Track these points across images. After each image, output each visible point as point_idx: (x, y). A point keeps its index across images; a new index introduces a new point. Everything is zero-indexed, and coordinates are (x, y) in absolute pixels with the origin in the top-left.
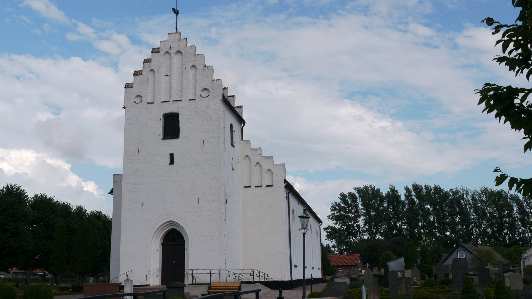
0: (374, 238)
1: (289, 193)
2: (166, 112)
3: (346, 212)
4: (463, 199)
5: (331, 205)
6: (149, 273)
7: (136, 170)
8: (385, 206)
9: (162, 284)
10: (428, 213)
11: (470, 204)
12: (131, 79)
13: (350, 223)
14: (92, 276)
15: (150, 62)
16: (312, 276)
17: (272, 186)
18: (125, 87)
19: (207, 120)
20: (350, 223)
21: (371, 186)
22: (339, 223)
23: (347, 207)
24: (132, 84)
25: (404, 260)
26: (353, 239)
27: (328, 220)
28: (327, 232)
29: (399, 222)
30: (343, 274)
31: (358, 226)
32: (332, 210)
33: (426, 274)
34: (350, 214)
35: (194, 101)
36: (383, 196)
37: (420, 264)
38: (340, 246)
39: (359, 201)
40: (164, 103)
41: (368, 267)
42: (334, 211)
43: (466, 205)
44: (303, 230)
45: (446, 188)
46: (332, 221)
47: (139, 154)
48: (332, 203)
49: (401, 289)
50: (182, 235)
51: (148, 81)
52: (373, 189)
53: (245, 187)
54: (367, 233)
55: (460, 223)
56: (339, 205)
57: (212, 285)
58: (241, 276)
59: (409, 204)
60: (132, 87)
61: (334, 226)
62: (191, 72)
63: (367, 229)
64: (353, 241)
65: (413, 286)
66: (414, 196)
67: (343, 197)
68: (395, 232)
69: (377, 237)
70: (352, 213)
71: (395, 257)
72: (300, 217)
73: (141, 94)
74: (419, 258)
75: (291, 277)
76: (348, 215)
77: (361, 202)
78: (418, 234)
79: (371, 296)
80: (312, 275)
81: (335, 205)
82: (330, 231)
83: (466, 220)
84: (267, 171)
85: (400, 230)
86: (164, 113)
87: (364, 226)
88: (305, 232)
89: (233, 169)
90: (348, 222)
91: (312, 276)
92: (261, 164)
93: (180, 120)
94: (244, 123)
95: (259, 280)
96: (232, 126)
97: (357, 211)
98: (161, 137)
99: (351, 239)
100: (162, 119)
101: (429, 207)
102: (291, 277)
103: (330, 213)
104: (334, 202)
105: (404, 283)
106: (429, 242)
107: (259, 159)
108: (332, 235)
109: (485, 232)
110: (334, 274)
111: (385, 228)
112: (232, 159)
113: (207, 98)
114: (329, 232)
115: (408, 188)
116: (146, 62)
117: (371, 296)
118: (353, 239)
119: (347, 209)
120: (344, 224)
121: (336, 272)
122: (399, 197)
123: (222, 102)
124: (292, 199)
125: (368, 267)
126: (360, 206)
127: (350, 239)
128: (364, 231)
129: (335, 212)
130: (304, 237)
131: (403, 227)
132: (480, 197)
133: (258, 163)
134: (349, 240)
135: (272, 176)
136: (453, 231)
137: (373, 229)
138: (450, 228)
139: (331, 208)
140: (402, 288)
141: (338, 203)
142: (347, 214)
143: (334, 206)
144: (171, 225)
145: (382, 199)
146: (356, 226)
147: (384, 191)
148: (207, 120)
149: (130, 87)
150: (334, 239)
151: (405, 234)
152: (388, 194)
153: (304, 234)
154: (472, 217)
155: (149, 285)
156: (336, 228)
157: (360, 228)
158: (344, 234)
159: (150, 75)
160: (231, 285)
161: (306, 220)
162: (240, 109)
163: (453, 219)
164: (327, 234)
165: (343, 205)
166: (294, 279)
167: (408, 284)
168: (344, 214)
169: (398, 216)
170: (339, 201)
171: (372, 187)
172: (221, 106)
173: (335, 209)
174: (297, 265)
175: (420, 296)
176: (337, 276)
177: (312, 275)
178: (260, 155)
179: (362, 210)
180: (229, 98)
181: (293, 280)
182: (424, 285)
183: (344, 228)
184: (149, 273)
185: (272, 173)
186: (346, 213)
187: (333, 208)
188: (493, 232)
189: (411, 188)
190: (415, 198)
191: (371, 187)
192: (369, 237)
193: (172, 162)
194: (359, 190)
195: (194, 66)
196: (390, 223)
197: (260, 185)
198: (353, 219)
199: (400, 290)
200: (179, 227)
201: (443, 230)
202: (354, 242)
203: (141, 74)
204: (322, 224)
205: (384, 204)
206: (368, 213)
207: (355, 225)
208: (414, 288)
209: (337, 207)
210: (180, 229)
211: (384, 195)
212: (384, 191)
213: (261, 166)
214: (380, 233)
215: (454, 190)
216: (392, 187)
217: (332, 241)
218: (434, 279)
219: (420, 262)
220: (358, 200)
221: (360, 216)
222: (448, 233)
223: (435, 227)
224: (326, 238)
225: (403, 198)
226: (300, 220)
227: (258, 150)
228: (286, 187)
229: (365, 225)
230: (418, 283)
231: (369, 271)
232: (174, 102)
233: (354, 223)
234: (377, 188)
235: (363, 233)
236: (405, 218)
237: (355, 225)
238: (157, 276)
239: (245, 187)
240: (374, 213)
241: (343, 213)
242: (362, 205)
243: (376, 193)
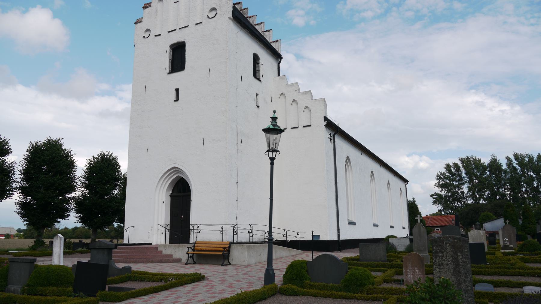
0: (478, 203)
1: (334, 135)
2: (172, 43)
3: (450, 180)
5: (436, 175)
6: (151, 230)
7: (143, 112)
8: (488, 174)
9: (169, 243)
10: (531, 179)
13: (455, 190)
16: (313, 234)
17: (310, 126)
19: (214, 44)
20: (455, 190)
22: (444, 190)
23: (452, 176)
25: (503, 220)
26: (458, 203)
27: (434, 187)
28: (434, 198)
29: (502, 188)
30: (439, 234)
31: (462, 193)
32: (437, 179)
33: (528, 234)
34: (454, 182)
35: (201, 24)
36: (485, 165)
37: (522, 224)
38: (446, 210)
39: (462, 170)
40: (171, 33)
41: (419, 221)
42: (439, 180)
44: (270, 153)
46: (438, 188)
47: (145, 94)
48: (438, 173)
49: (442, 264)
50: (186, 181)
51: (157, 12)
52: (475, 160)
54: (471, 199)
56: (444, 174)
57: (196, 245)
58: (192, 230)
60: (141, 22)
61: (439, 193)
63: (471, 195)
64: (458, 206)
65: (502, 251)
66: (516, 164)
67: (448, 167)
68: (498, 197)
69: (481, 202)
70: (456, 181)
71: (495, 218)
72: (265, 130)
73: (150, 28)
74: (521, 219)
75: (339, 236)
76: (452, 183)
77: (464, 171)
78: (521, 199)
79: (409, 270)
80: (313, 232)
81: (440, 174)
82: (436, 197)
84: (280, 95)
85: (504, 195)
86: (171, 44)
87: (468, 193)
88: (274, 156)
89: (258, 107)
90: (453, 190)
91: (313, 234)
92: (297, 102)
93: (186, 49)
94: (281, 58)
95: (336, 238)
96: (256, 59)
97: (461, 179)
98: (168, 71)
99: (456, 204)
100: (168, 51)
101: (532, 173)
102: (339, 236)
103: (436, 182)
105: (448, 250)
106: (533, 206)
107: (295, 96)
108: (438, 201)
110: (430, 234)
111: (488, 194)
112: (257, 95)
113: (214, 18)
114: (435, 198)
115: (509, 158)
117: (409, 270)
118: (458, 203)
119: (452, 177)
120: (449, 191)
121: (431, 232)
122: (500, 166)
123: (233, 22)
124: (339, 141)
125: (419, 221)
126: (464, 175)
127: (455, 203)
128: (467, 197)
129: (441, 180)
130: (272, 164)
131: (507, 192)
133: (294, 100)
134: (454, 205)
135: (311, 114)
137: (476, 195)
139: (437, 177)
140: (444, 262)
141: (442, 173)
142: (452, 182)
143: (440, 175)
144: (176, 172)
145: (484, 168)
146: (460, 193)
147: (486, 161)
148: (214, 44)
149: (139, 22)
150: (440, 204)
151: (508, 199)
153: (272, 159)
155: (151, 244)
156: (442, 194)
157: (464, 194)
158: (449, 200)
160: (208, 245)
161: (273, 137)
162: (277, 44)
164: (433, 200)
165: (447, 174)
166: (342, 238)
167: (459, 254)
168: (449, 182)
169: (501, 182)
170: (444, 171)
171: (474, 158)
172: (233, 29)
173: (440, 178)
174: (405, 227)
175: (510, 270)
176: (432, 236)
177: (313, 232)
178: (296, 90)
179: (466, 178)
180: (265, 32)
181: (341, 239)
182: (521, 250)
183: (449, 194)
184: (151, 230)
185: (310, 110)
186: (450, 182)
187: (438, 177)
189: (512, 158)
190: (517, 166)
191: (473, 158)
192: (472, 202)
193: (177, 99)
194: (463, 161)
196: (493, 190)
197: (297, 126)
198: (458, 186)
199: (439, 268)
200: (183, 173)
202: (459, 207)
204: (407, 183)
205: (487, 172)
206: (471, 181)
207: (459, 192)
208: (504, 254)
209: (442, 176)
210: (185, 177)
211: (486, 164)
212: (486, 161)
213: (297, 104)
214: (483, 198)
216: (494, 157)
217: (438, 206)
218: (538, 241)
219: (523, 222)
220: (462, 170)
221: (463, 184)
224: (433, 203)
225: (504, 167)
226: (266, 135)
227: (293, 85)
228: (327, 126)
229: (469, 191)
230: (512, 246)
231: (422, 228)
232: (180, 30)
233: (458, 190)
234: (478, 159)
235: (467, 199)
236: (508, 185)
237: (459, 192)
238: (162, 233)
240: (477, 181)
241: (448, 181)
242: (465, 174)
243: (477, 163)
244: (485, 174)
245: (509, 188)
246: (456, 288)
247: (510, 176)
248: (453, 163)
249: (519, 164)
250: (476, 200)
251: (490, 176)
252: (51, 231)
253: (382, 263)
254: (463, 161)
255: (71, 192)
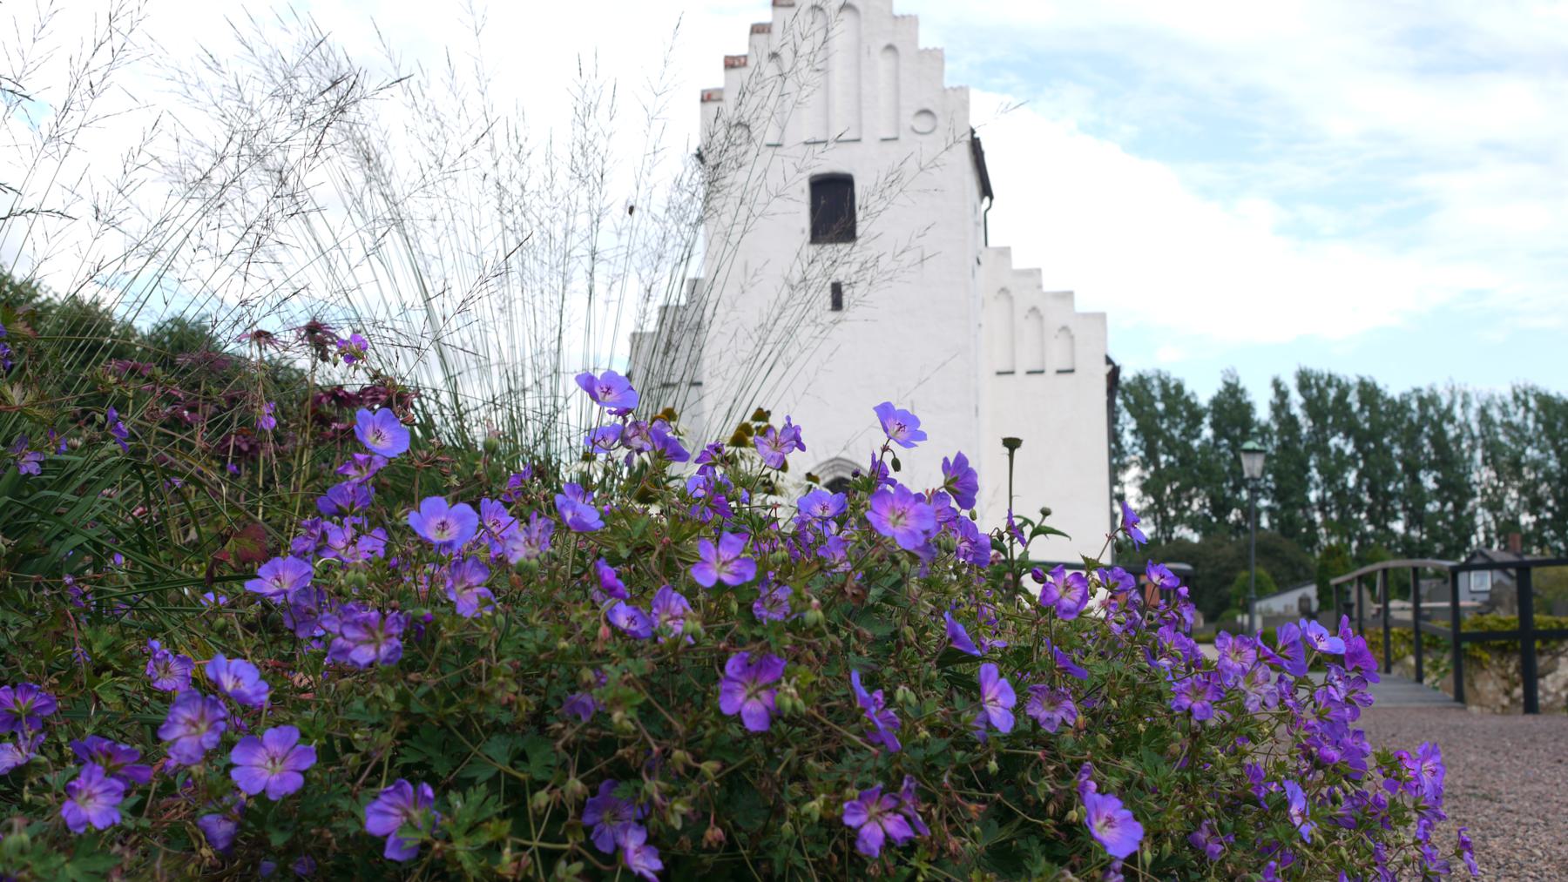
4: (1452, 420)
10: (1343, 462)
11: (1473, 438)
12: (716, 78)
14: (1424, 508)
15: (769, 31)
17: (1072, 371)
18: (703, 100)
21: (1159, 372)
24: (720, 91)
43: (1458, 439)
45: (1394, 387)
52: (1164, 384)
53: (999, 373)
55: (1437, 494)
59: (1280, 433)
62: (883, 64)
71: (1274, 588)
83: (1456, 488)
104: (788, 418)
109: (1516, 523)
116: (758, 32)
122: (1248, 408)
132: (1505, 413)
136: (1416, 518)
138: (1405, 509)
145: (1195, 416)
147: (1204, 391)
152: (1217, 403)
154: (1475, 477)
159: (770, 70)
163: (1416, 481)
188: (1539, 524)
195: (890, 48)
201: (1381, 516)
203: (745, 65)
206: (1151, 456)
212: (1204, 391)
215: (1425, 395)
221: (1125, 467)
222: (1398, 526)
223: (1359, 506)
239: (999, 373)
243: (1175, 395)
244: (1197, 436)
245: (1269, 488)
246: (1338, 848)
247: (1278, 448)
248: (1226, 383)
249: (1311, 407)
250: (1166, 524)
251: (1216, 446)
252: (939, 511)
253: (484, 668)
254: (1304, 381)
255: (164, 334)
